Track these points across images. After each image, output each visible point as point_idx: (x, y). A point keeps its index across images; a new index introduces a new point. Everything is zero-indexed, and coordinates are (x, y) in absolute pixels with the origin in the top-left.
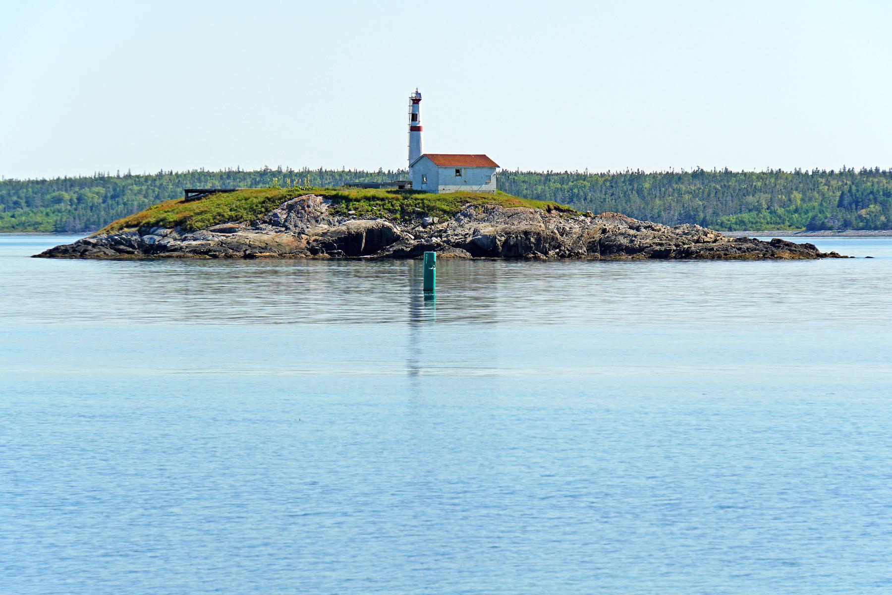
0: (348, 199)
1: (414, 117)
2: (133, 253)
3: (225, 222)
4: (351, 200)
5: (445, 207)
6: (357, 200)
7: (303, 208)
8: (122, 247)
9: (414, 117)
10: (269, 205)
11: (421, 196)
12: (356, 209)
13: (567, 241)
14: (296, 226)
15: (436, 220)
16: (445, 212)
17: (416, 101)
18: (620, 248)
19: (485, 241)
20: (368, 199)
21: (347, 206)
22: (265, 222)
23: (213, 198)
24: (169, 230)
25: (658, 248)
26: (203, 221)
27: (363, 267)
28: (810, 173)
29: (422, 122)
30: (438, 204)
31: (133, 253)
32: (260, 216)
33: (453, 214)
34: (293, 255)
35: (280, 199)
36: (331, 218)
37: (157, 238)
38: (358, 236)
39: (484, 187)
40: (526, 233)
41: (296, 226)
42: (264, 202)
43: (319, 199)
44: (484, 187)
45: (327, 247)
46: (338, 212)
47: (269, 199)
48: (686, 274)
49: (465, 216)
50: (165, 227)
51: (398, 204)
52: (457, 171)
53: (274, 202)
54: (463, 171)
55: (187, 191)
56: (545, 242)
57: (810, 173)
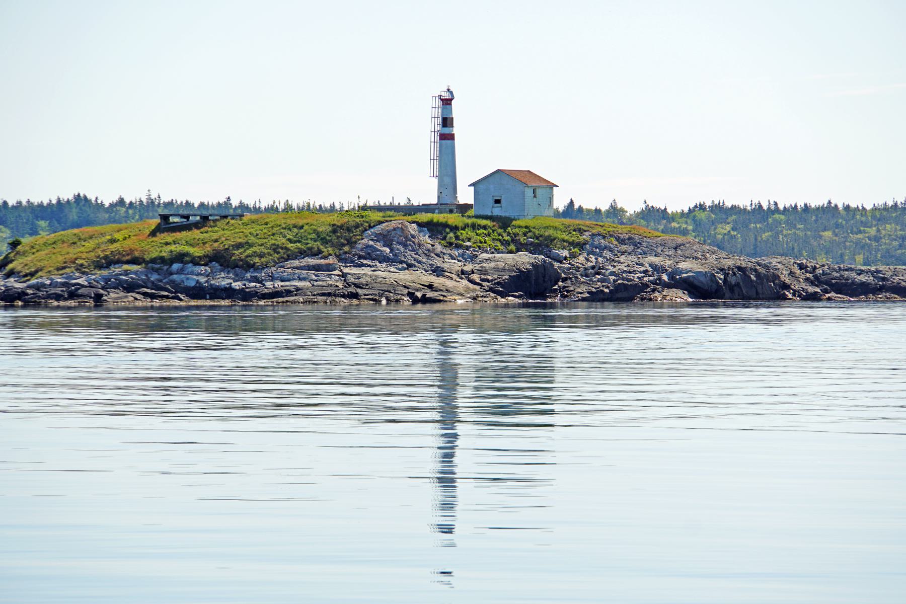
0: (455, 229)
1: (447, 122)
16: (572, 244)
17: (447, 102)
19: (702, 279)
21: (457, 238)
22: (360, 257)
29: (457, 130)
32: (346, 249)
41: (420, 262)
47: (341, 227)
56: (768, 280)
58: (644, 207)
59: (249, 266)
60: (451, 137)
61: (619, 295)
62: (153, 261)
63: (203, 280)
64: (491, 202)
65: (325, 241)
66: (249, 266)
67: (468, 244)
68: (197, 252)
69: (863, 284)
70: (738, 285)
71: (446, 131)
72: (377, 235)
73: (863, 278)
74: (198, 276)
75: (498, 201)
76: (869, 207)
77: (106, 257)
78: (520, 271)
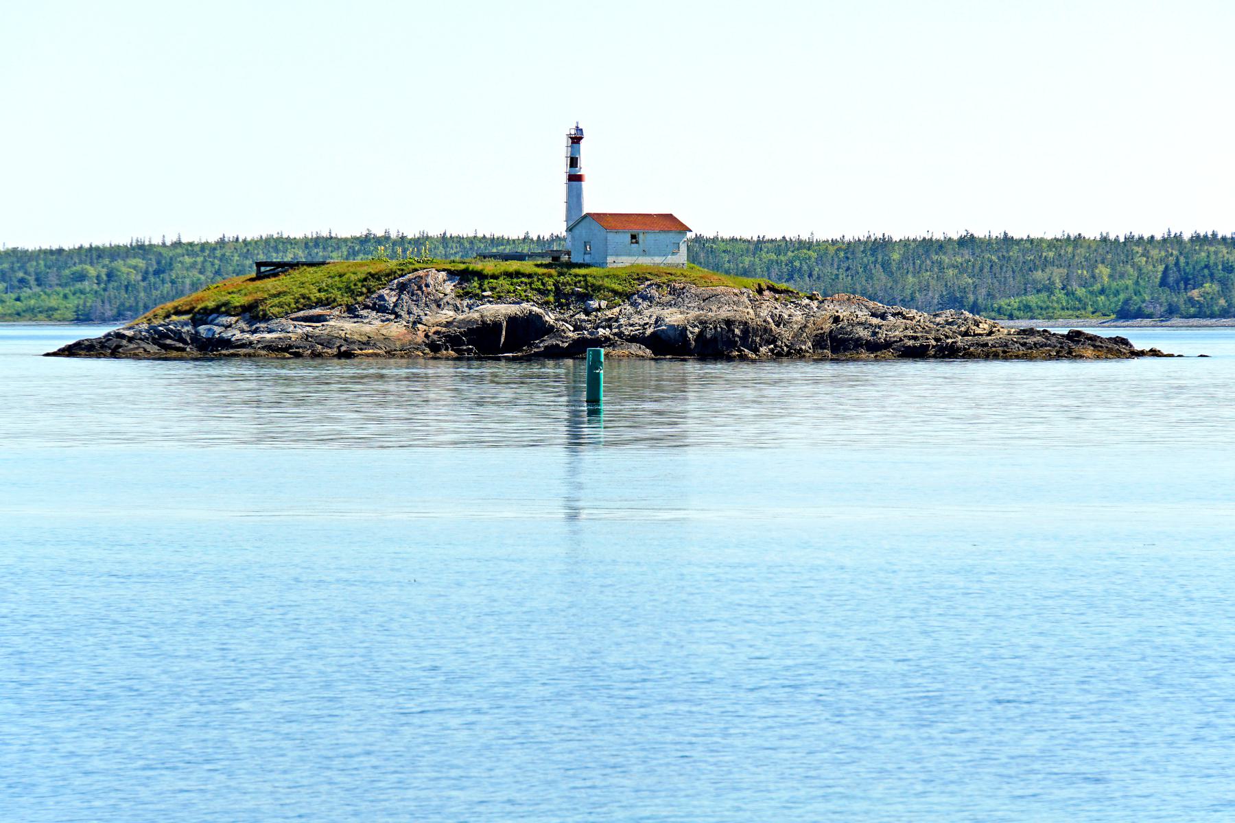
0: (481, 276)
1: (574, 162)
2: (184, 350)
3: (311, 308)
6: (495, 277)
7: (420, 288)
8: (169, 342)
9: (574, 162)
10: (372, 283)
11: (583, 271)
12: (492, 289)
14: (409, 313)
15: (604, 304)
16: (615, 293)
17: (576, 140)
19: (671, 333)
22: (366, 307)
23: (295, 273)
24: (234, 319)
25: (911, 343)
28: (1122, 240)
29: (584, 168)
31: (184, 350)
32: (360, 299)
33: (627, 296)
35: (388, 275)
36: (458, 302)
37: (217, 329)
38: (497, 326)
39: (671, 259)
41: (409, 313)
42: (365, 280)
43: (442, 275)
44: (671, 259)
45: (453, 341)
46: (467, 293)
49: (644, 298)
50: (228, 314)
51: (551, 282)
52: (633, 237)
53: (379, 279)
54: (641, 237)
55: (259, 265)
57: (1122, 240)
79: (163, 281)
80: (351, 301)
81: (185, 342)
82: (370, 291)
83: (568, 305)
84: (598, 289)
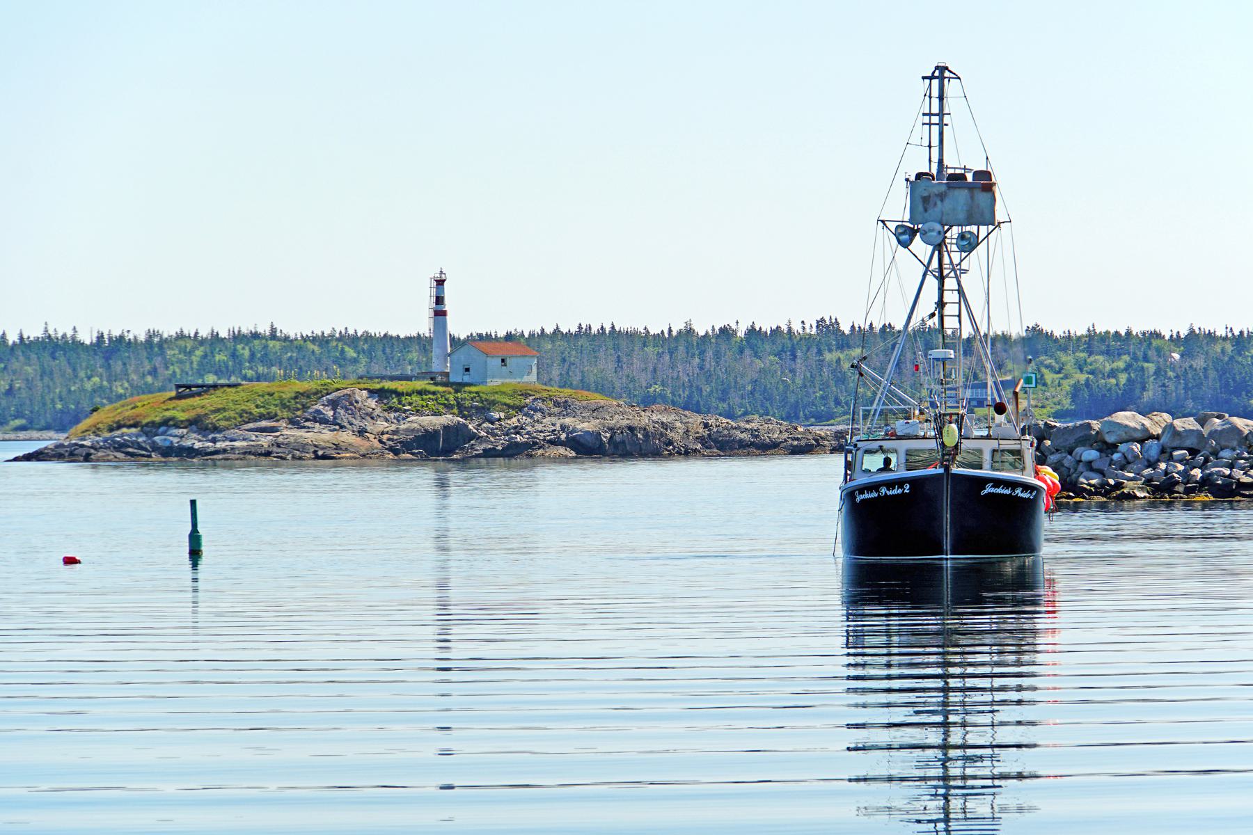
0: (399, 394)
1: (439, 300)
2: (150, 456)
3: (256, 421)
4: (402, 394)
5: (508, 401)
6: (409, 395)
7: (351, 404)
8: (130, 450)
9: (439, 300)
10: (304, 401)
11: (473, 389)
12: (410, 404)
13: (675, 436)
14: (351, 424)
15: (502, 415)
16: (509, 406)
17: (440, 283)
18: (742, 445)
19: (588, 438)
20: (420, 393)
21: (400, 402)
22: (307, 420)
23: (219, 392)
24: (185, 431)
25: (796, 443)
26: (228, 419)
27: (573, 466)
28: (526, 335)
29: (448, 306)
30: (497, 397)
31: (150, 456)
32: (299, 413)
33: (519, 409)
34: (364, 459)
35: (316, 394)
36: (386, 414)
37: (175, 440)
38: (436, 432)
39: (526, 379)
40: (631, 428)
41: (351, 424)
42: (296, 398)
43: (365, 393)
44: (526, 379)
45: (407, 446)
46: (391, 408)
47: (302, 394)
48: (47, 471)
49: (535, 410)
50: (178, 427)
51: (451, 397)
52: (503, 361)
53: (308, 397)
54: (508, 361)
55: (178, 387)
56: (654, 438)
57: (526, 335)
58: (69, 334)
59: (216, 429)
60: (444, 313)
61: (510, 452)
62: (147, 425)
63: (175, 440)
64: (461, 370)
65: (284, 406)
66: (216, 429)
67: (407, 407)
68: (182, 416)
69: (741, 441)
70: (623, 442)
71: (440, 308)
72: (329, 401)
73: (743, 436)
74: (174, 437)
75: (467, 370)
76: (402, 336)
77: (118, 422)
78: (426, 431)
79: (742, 397)
80: (291, 415)
81: (145, 449)
82: (305, 407)
83: (471, 416)
84: (494, 403)
